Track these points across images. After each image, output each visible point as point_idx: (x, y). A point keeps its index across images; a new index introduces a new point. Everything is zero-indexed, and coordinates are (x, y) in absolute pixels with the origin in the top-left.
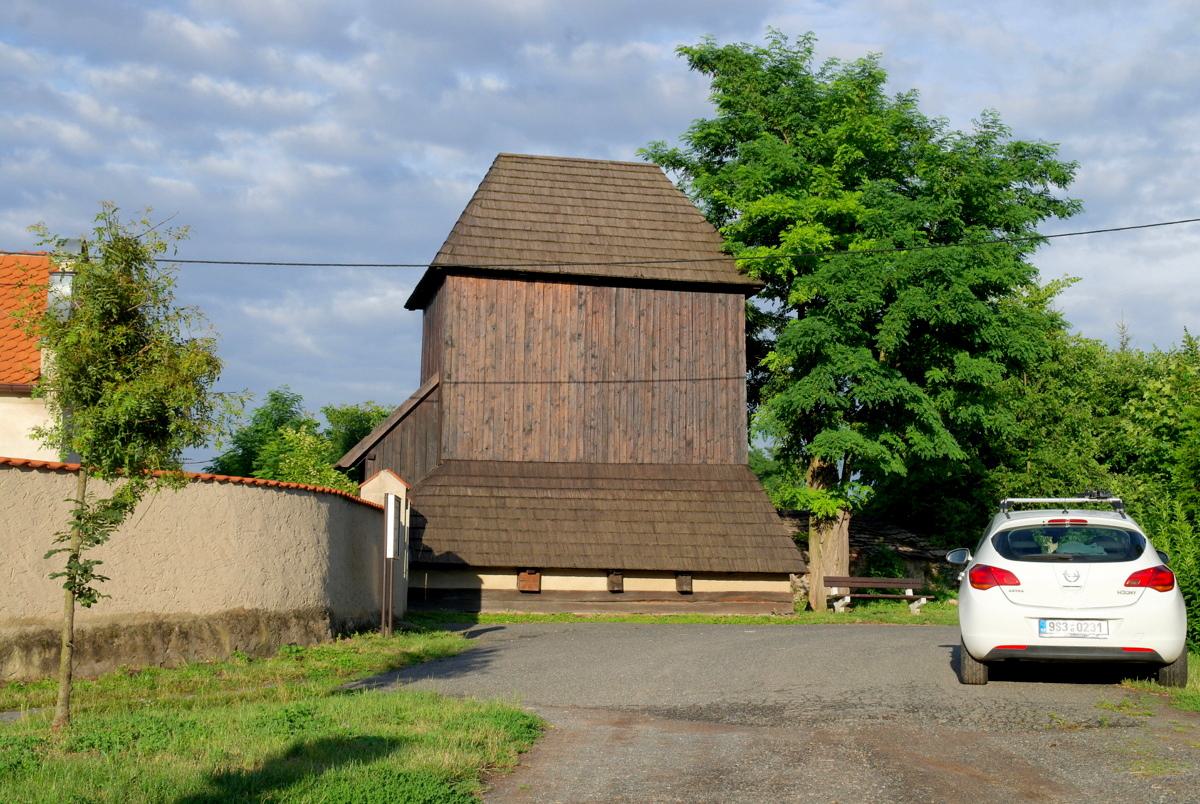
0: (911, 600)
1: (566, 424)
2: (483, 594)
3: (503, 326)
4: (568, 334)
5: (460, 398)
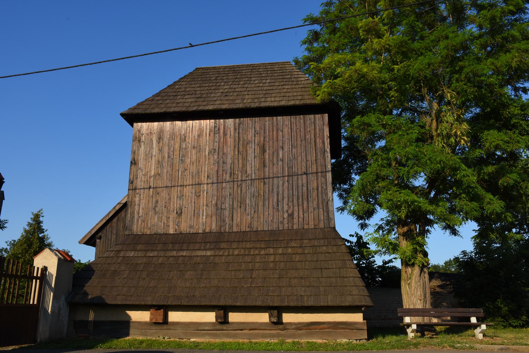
0: (475, 326)
2: (131, 324)
4: (207, 150)
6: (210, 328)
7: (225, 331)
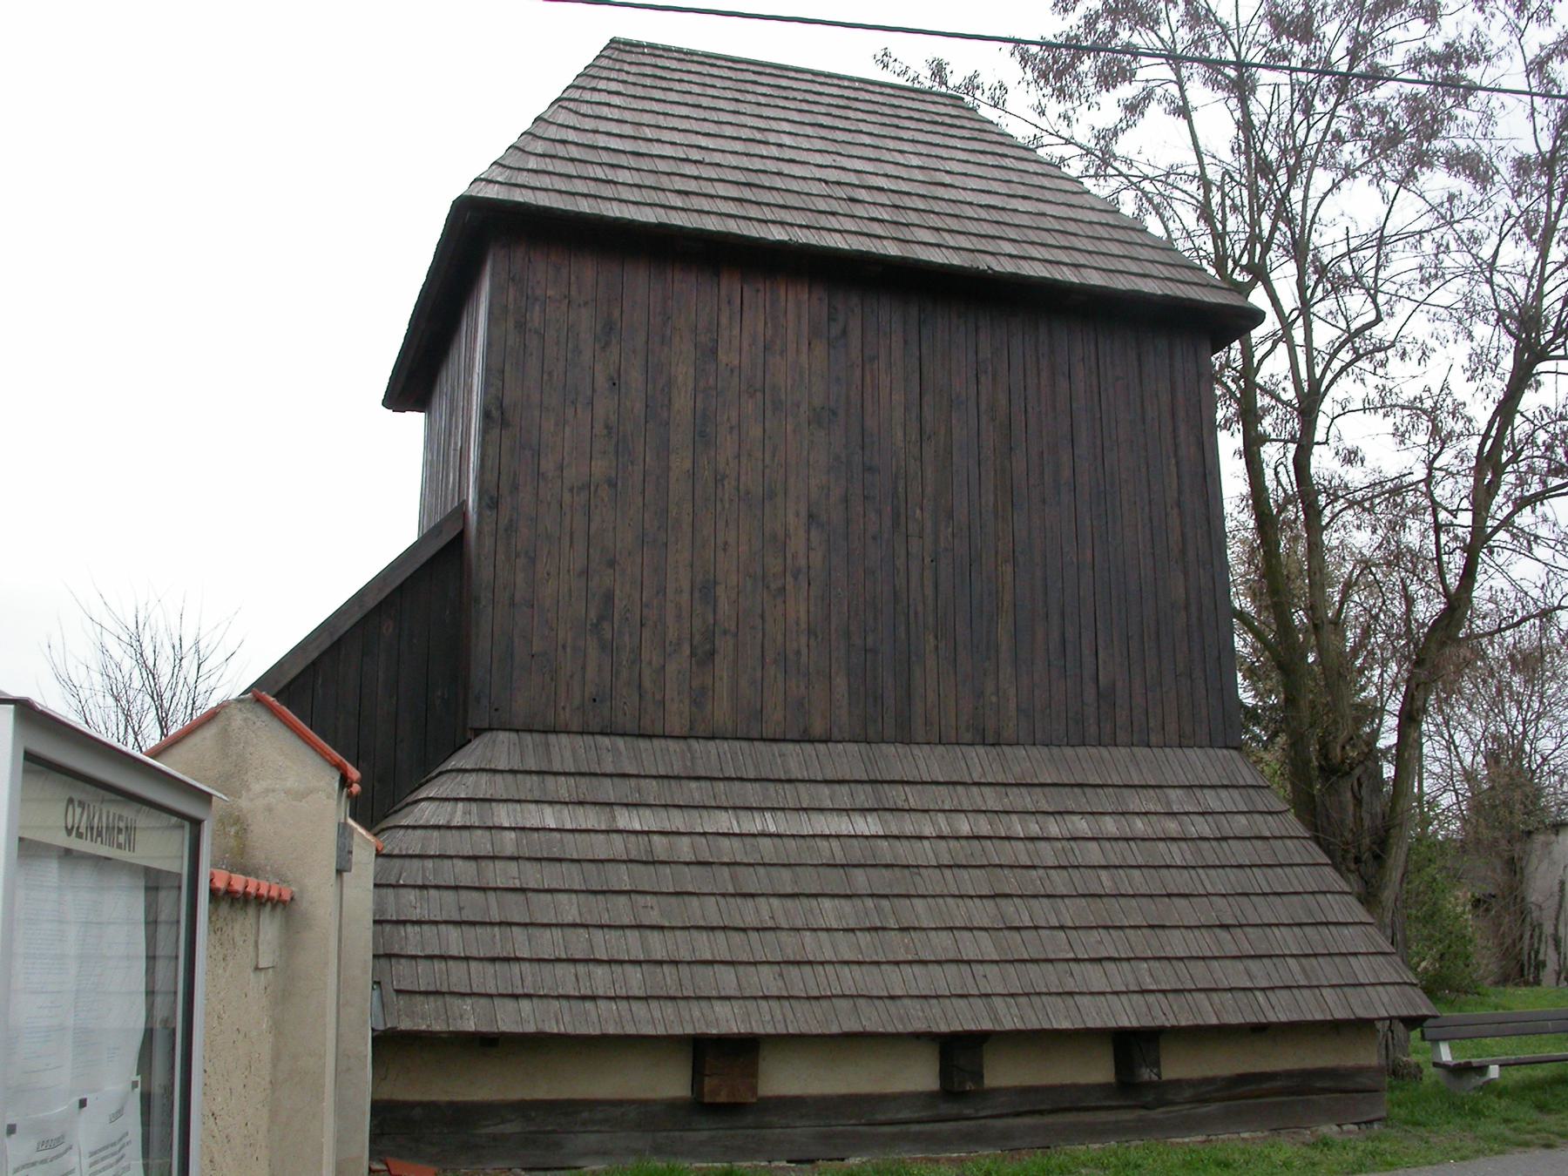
1: (803, 640)
3: (635, 377)
5: (522, 561)
6: (916, 1115)
7: (967, 1123)
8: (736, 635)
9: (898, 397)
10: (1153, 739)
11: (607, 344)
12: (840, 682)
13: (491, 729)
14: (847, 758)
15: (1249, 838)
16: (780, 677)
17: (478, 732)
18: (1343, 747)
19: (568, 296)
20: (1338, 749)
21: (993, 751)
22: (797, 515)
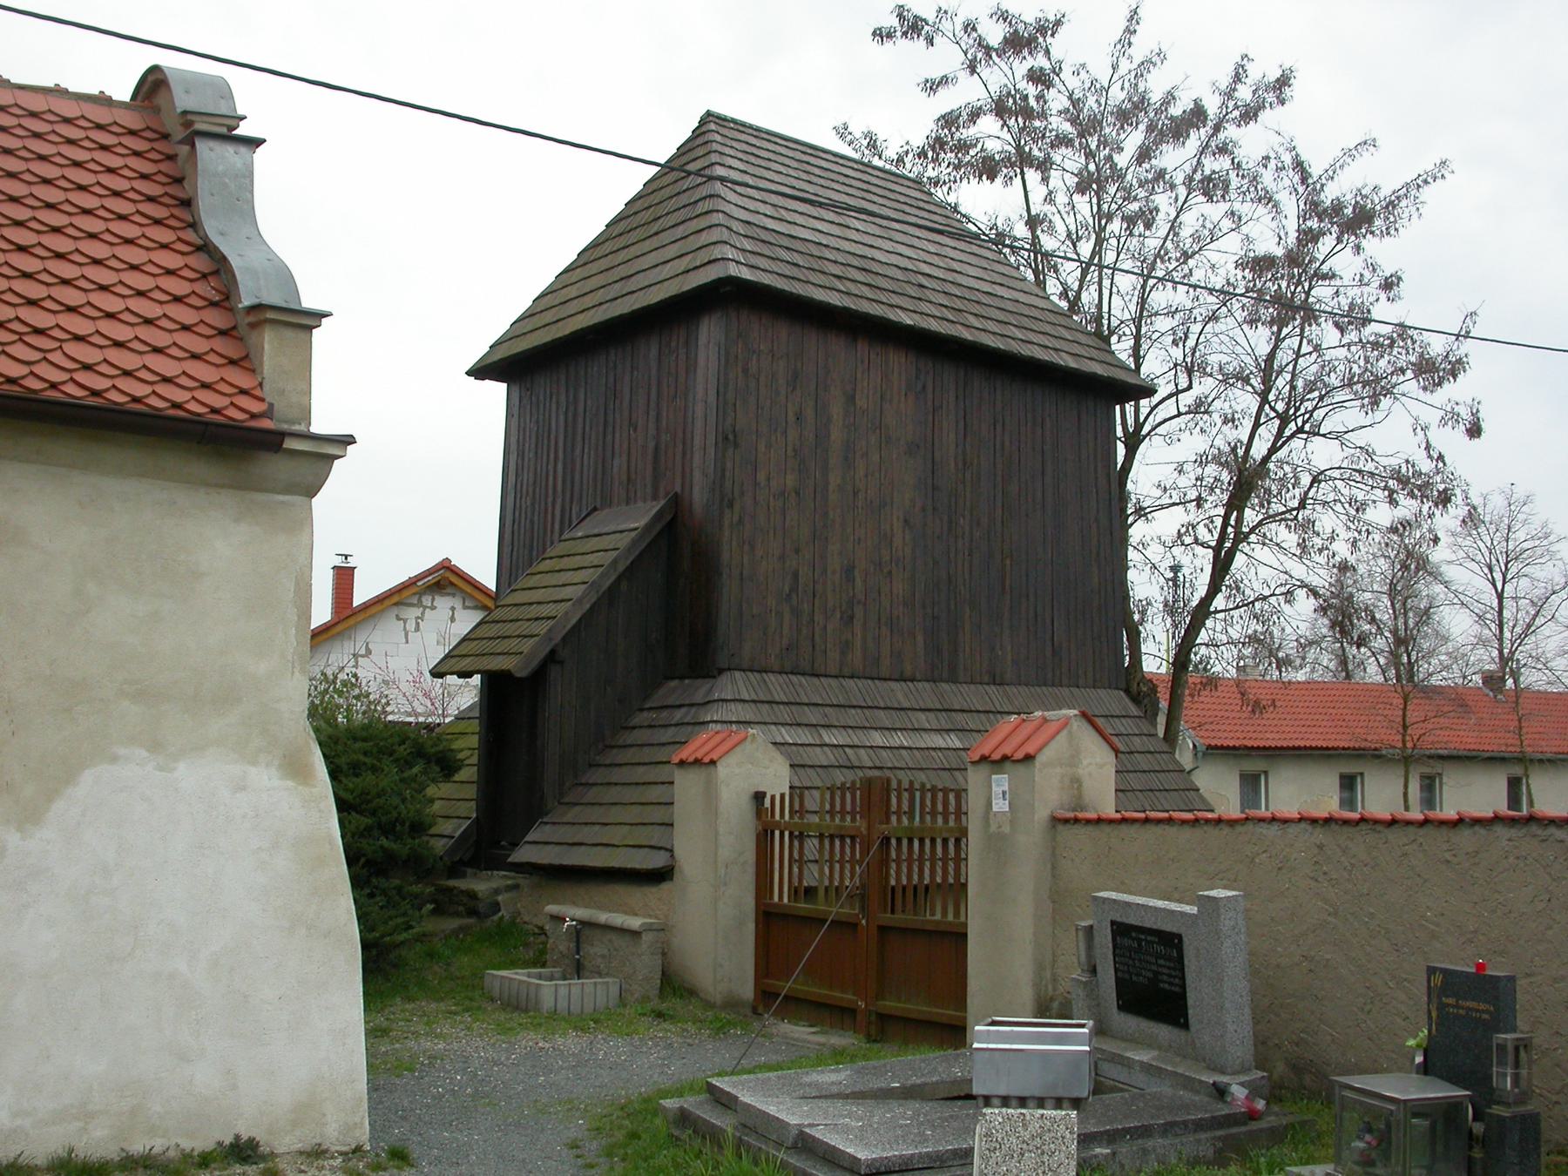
8: (865, 604)
9: (952, 436)
10: (1081, 682)
11: (794, 388)
12: (920, 638)
13: (729, 669)
14: (925, 692)
15: (1143, 753)
16: (889, 634)
17: (721, 671)
18: (1138, 684)
19: (772, 351)
20: (1136, 685)
21: (1001, 689)
22: (898, 519)
